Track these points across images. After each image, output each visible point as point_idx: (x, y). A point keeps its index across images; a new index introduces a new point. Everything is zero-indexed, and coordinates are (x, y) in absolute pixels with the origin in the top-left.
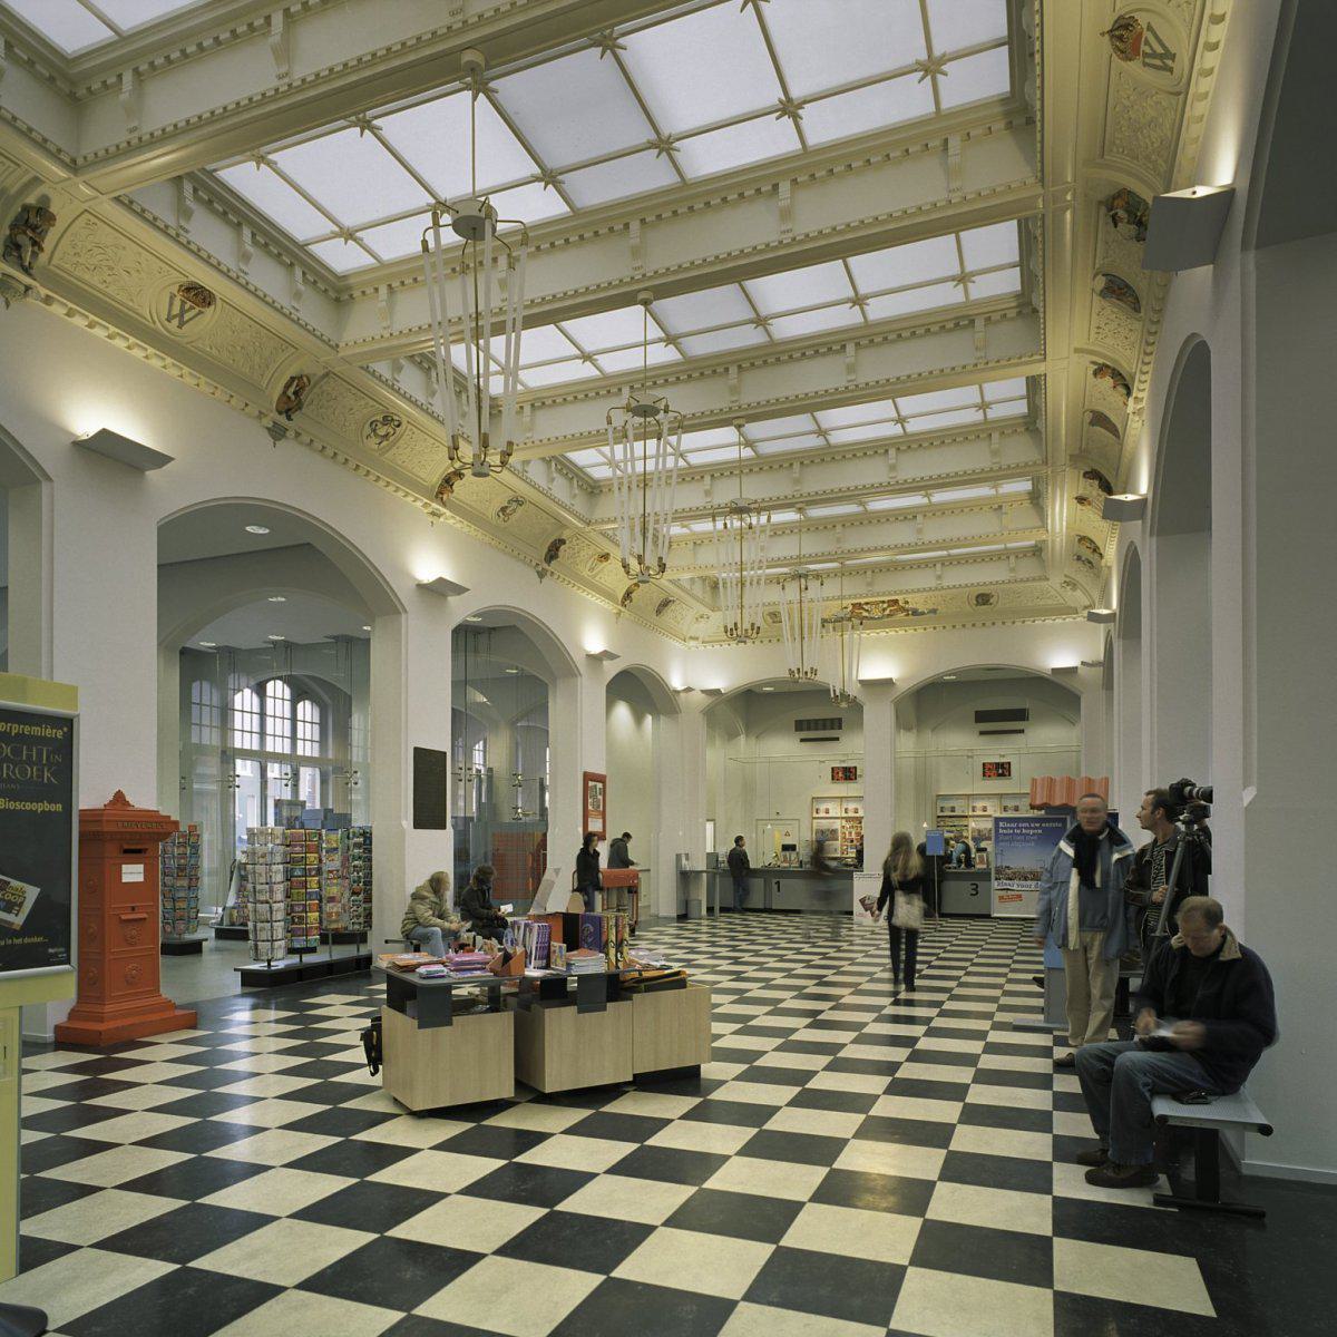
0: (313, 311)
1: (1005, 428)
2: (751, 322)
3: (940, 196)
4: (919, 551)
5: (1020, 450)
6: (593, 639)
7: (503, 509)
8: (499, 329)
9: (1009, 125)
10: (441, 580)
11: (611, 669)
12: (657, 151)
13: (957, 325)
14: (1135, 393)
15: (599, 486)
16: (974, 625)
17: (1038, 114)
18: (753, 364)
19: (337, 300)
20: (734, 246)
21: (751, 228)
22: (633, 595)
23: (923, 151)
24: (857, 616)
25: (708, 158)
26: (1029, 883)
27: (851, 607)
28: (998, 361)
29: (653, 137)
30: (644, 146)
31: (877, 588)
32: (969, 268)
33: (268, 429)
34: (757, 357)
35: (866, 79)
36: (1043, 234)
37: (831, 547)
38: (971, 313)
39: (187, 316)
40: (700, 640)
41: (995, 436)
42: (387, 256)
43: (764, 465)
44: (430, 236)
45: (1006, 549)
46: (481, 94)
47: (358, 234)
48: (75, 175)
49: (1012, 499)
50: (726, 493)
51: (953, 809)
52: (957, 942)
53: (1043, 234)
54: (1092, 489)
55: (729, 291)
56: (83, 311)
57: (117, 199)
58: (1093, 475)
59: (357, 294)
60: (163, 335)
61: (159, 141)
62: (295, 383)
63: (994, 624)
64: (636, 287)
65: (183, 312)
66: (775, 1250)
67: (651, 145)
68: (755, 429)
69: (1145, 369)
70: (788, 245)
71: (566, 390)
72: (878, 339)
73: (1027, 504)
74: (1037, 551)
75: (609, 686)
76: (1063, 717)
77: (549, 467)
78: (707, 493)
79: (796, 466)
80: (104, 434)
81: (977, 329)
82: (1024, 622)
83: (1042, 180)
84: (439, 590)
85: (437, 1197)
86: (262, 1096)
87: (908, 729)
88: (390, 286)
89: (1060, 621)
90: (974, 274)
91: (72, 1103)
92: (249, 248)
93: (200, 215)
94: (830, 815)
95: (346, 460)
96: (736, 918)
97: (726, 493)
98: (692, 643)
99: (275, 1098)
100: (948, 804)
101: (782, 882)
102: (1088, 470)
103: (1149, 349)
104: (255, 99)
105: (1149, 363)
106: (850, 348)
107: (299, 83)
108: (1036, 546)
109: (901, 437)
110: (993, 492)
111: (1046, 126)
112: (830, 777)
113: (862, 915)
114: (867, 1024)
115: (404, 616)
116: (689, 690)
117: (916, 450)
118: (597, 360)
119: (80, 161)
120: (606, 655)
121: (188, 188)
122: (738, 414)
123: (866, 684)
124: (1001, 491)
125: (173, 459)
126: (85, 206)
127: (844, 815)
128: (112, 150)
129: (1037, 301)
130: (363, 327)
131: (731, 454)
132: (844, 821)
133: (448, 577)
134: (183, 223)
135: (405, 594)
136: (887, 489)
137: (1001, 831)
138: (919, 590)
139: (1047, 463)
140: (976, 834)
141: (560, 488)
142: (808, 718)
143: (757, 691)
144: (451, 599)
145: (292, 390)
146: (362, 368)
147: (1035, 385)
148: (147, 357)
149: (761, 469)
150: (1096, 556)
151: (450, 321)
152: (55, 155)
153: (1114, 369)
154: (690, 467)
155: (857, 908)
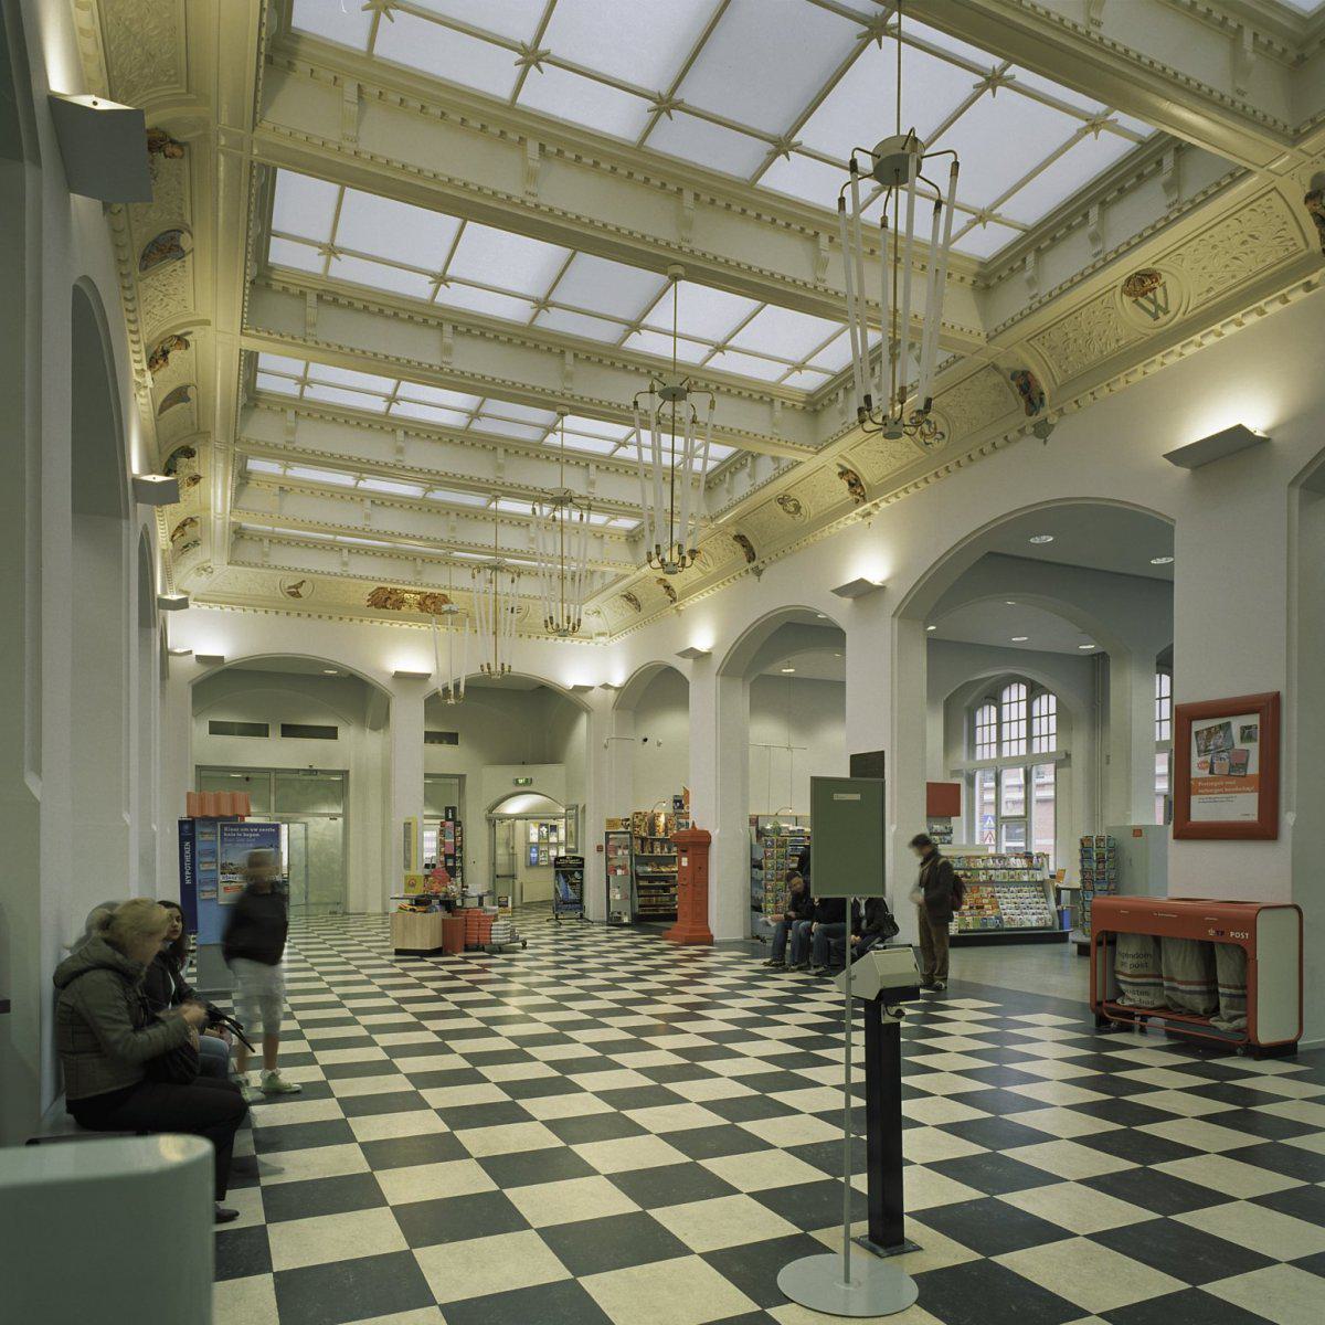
4: (522, 558)
16: (320, 617)
18: (625, 367)
20: (746, 259)
21: (783, 257)
24: (385, 601)
30: (766, 137)
34: (544, 342)
39: (1161, 301)
44: (848, 194)
45: (334, 541)
49: (613, 533)
63: (341, 619)
65: (1154, 302)
71: (724, 380)
82: (361, 621)
86: (956, 1076)
89: (416, 628)
90: (342, 251)
98: (602, 639)
102: (735, 533)
117: (434, 441)
123: (399, 676)
124: (290, 473)
128: (1216, 95)
149: (440, 439)
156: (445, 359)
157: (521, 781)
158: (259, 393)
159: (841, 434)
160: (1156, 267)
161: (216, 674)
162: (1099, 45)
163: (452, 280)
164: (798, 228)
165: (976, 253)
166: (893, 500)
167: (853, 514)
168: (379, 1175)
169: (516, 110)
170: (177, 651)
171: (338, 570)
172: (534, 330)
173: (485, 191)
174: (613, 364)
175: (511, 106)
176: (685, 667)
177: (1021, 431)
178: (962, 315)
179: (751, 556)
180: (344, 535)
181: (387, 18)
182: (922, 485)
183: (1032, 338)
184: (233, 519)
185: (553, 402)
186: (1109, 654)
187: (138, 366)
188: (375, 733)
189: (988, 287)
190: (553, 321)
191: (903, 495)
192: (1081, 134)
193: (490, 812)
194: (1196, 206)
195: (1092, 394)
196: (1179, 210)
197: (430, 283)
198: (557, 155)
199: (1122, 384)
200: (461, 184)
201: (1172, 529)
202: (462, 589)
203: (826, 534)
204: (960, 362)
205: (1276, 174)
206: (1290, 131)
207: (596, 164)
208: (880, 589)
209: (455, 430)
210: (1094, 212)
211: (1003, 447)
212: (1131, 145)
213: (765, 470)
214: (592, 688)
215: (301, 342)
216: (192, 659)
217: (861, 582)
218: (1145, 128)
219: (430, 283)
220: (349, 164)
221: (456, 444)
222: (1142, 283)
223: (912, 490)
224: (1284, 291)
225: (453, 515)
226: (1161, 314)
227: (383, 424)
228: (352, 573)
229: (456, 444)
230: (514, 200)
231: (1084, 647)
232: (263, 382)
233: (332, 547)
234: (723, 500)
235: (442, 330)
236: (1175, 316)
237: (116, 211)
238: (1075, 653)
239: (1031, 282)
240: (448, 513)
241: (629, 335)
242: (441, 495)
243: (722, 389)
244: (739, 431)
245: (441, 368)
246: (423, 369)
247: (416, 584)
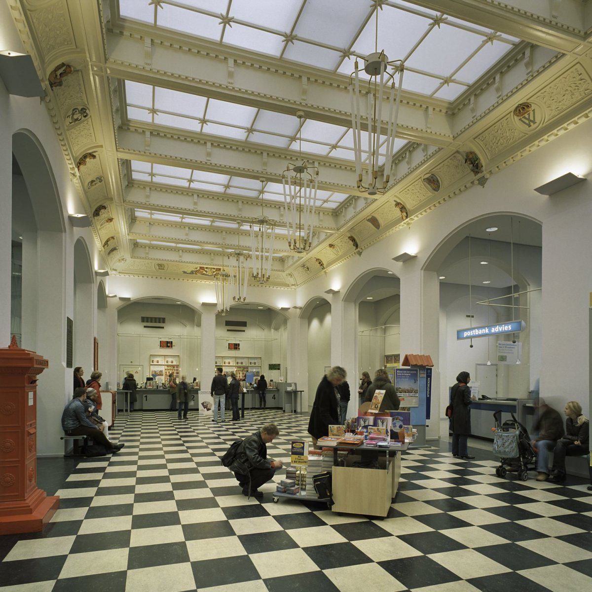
7: (92, 181)
8: (384, 131)
15: (133, 183)
18: (274, 155)
22: (109, 243)
24: (200, 272)
26: (407, 394)
27: (199, 268)
29: (224, 13)
35: (249, 23)
37: (221, 241)
39: (532, 118)
51: (158, 362)
59: (127, 33)
61: (580, 36)
62: (64, 68)
64: (300, 108)
65: (528, 119)
66: (251, 554)
76: (181, 322)
85: (398, 537)
90: (208, 121)
94: (159, 363)
96: (259, 412)
100: (240, 361)
101: (148, 396)
102: (350, 236)
109: (149, 183)
112: (228, 347)
113: (202, 410)
115: (64, 234)
122: (265, 176)
123: (204, 304)
127: (166, 364)
132: (166, 366)
136: (131, 204)
137: (398, 374)
140: (154, 373)
142: (152, 317)
145: (61, 71)
151: (382, 121)
153: (403, 206)
155: (201, 407)
156: (208, 159)
158: (134, 180)
160: (528, 101)
161: (128, 305)
162: (505, 9)
163: (255, 131)
164: (344, 87)
166: (420, 216)
167: (402, 223)
169: (223, 45)
170: (110, 295)
171: (178, 259)
172: (290, 151)
174: (286, 157)
175: (221, 43)
176: (329, 298)
177: (472, 183)
178: (440, 128)
179: (356, 245)
180: (181, 243)
182: (433, 208)
183: (476, 137)
184: (130, 238)
185: (258, 176)
186: (519, 286)
187: (71, 166)
189: (454, 114)
190: (256, 138)
191: (424, 213)
192: (485, 42)
194: (539, 73)
195: (505, 162)
196: (532, 76)
197: (199, 123)
198: (243, 64)
199: (519, 157)
201: (541, 226)
203: (391, 233)
204: (441, 151)
205: (578, 55)
206: (582, 33)
208: (415, 257)
209: (219, 193)
210: (498, 77)
211: (464, 191)
212: (510, 47)
213: (361, 204)
214: (289, 309)
215: (133, 152)
216: (117, 298)
217: (405, 254)
218: (517, 40)
219: (158, 115)
220: (120, 68)
221: (215, 199)
222: (522, 109)
223: (428, 211)
224: (587, 112)
225: (224, 233)
226: (532, 124)
227: (187, 192)
228: (183, 260)
232: (135, 176)
233: (176, 250)
234: (342, 221)
235: (262, 156)
236: (539, 126)
237: (48, 101)
238: (365, 300)
239: (473, 110)
240: (222, 232)
241: (291, 143)
242: (219, 224)
243: (337, 166)
244: (342, 185)
246: (212, 166)
247: (211, 265)
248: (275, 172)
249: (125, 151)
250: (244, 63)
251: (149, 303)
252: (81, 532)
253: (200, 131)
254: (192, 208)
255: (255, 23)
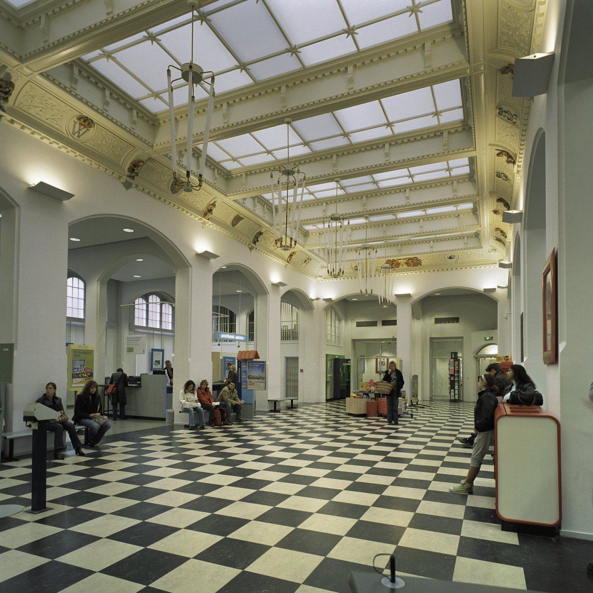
0: (141, 129)
1: (460, 179)
2: (341, 135)
3: (421, 69)
5: (467, 190)
6: (275, 277)
9: (453, 36)
10: (206, 252)
11: (283, 290)
12: (291, 53)
13: (435, 135)
14: (517, 163)
17: (465, 28)
19: (153, 125)
21: (334, 87)
23: (414, 50)
24: (393, 265)
25: (313, 56)
28: (453, 151)
29: (346, 27)
31: (403, 253)
32: (439, 109)
33: (123, 183)
36: (471, 86)
38: (441, 129)
39: (81, 132)
40: (323, 277)
41: (455, 183)
42: (246, 165)
43: (348, 198)
46: (204, 22)
47: (161, 95)
48: (22, 63)
49: (464, 212)
50: (331, 210)
52: (440, 415)
53: (471, 86)
54: (501, 207)
55: (326, 117)
56: (39, 132)
57: (41, 74)
58: (500, 200)
60: (73, 141)
67: (288, 51)
68: (345, 182)
69: (521, 152)
70: (352, 95)
72: (399, 142)
73: (471, 214)
74: (477, 235)
75: (282, 298)
77: (132, 113)
78: (324, 211)
79: (364, 198)
80: (41, 184)
81: (444, 137)
83: (469, 61)
84: (206, 257)
87: (418, 319)
88: (47, 14)
91: (181, 461)
92: (108, 99)
93: (113, 104)
95: (165, 200)
97: (331, 210)
98: (320, 278)
99: (274, 452)
103: (523, 143)
104: (97, 25)
105: (523, 149)
106: (387, 146)
107: (116, 16)
108: (477, 233)
110: (455, 209)
111: (469, 39)
114: (360, 475)
115: (190, 268)
116: (318, 299)
117: (393, 193)
118: (273, 153)
119: (24, 57)
120: (281, 284)
121: (76, 70)
123: (398, 296)
124: (459, 208)
125: (74, 195)
126: (28, 79)
129: (470, 123)
130: (163, 138)
131: (333, 193)
133: (210, 250)
134: (73, 86)
135: (190, 258)
138: (422, 253)
139: (478, 195)
141: (259, 210)
143: (349, 300)
144: (212, 260)
146: (164, 155)
147: (472, 161)
148: (68, 152)
150: (504, 237)
152: (12, 54)
154: (317, 199)
157: (488, 338)
159: (219, 189)
165: (445, 21)
168: (411, 514)
169: (362, 52)
173: (263, 116)
175: (359, 52)
180: (439, 234)
181: (420, 13)
188: (418, 321)
193: (477, 354)
200: (275, 113)
202: (425, 253)
207: (316, 77)
219: (441, 116)
225: (385, 225)
229: (424, 189)
230: (294, 108)
231: (138, 276)
245: (333, 174)
248: (362, 166)
249: (465, 150)
250: (234, 101)
251: (450, 296)
252: (385, 493)
253: (392, 134)
254: (453, 196)
255: (384, 15)
